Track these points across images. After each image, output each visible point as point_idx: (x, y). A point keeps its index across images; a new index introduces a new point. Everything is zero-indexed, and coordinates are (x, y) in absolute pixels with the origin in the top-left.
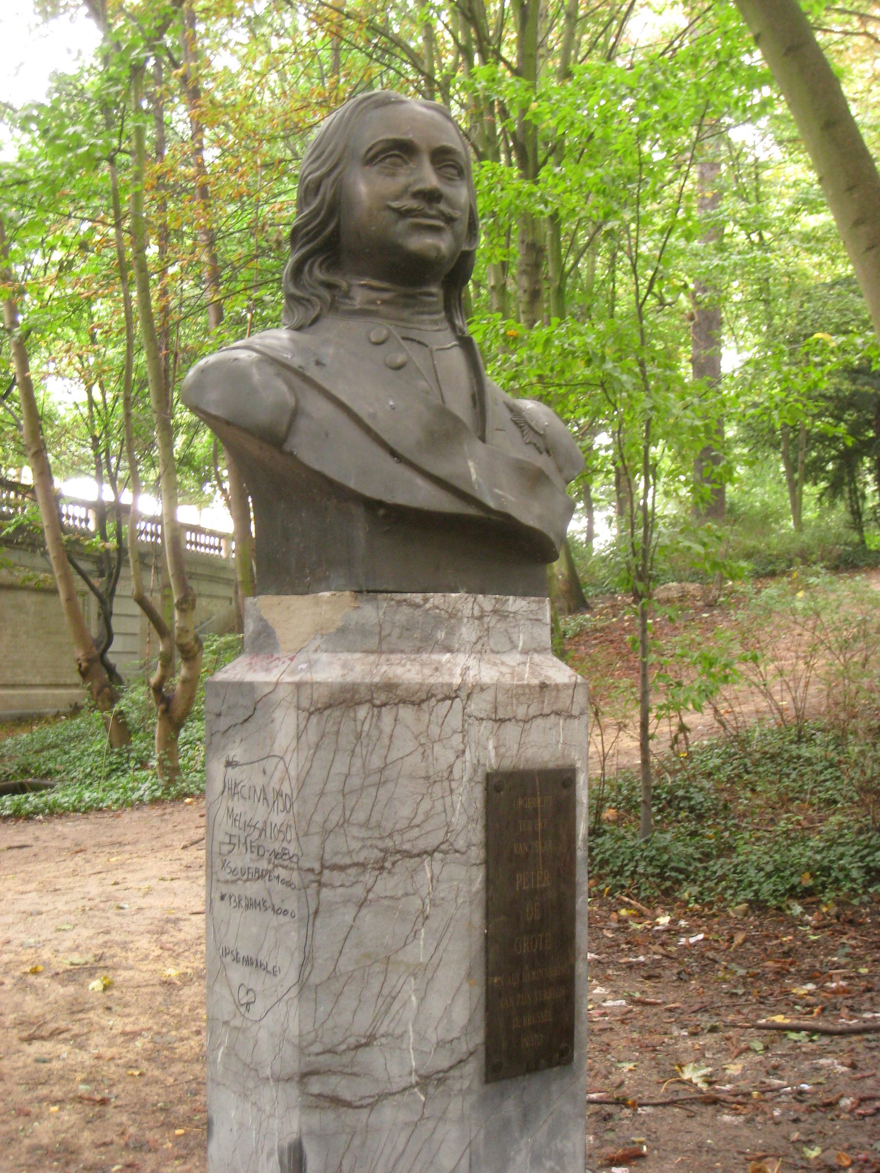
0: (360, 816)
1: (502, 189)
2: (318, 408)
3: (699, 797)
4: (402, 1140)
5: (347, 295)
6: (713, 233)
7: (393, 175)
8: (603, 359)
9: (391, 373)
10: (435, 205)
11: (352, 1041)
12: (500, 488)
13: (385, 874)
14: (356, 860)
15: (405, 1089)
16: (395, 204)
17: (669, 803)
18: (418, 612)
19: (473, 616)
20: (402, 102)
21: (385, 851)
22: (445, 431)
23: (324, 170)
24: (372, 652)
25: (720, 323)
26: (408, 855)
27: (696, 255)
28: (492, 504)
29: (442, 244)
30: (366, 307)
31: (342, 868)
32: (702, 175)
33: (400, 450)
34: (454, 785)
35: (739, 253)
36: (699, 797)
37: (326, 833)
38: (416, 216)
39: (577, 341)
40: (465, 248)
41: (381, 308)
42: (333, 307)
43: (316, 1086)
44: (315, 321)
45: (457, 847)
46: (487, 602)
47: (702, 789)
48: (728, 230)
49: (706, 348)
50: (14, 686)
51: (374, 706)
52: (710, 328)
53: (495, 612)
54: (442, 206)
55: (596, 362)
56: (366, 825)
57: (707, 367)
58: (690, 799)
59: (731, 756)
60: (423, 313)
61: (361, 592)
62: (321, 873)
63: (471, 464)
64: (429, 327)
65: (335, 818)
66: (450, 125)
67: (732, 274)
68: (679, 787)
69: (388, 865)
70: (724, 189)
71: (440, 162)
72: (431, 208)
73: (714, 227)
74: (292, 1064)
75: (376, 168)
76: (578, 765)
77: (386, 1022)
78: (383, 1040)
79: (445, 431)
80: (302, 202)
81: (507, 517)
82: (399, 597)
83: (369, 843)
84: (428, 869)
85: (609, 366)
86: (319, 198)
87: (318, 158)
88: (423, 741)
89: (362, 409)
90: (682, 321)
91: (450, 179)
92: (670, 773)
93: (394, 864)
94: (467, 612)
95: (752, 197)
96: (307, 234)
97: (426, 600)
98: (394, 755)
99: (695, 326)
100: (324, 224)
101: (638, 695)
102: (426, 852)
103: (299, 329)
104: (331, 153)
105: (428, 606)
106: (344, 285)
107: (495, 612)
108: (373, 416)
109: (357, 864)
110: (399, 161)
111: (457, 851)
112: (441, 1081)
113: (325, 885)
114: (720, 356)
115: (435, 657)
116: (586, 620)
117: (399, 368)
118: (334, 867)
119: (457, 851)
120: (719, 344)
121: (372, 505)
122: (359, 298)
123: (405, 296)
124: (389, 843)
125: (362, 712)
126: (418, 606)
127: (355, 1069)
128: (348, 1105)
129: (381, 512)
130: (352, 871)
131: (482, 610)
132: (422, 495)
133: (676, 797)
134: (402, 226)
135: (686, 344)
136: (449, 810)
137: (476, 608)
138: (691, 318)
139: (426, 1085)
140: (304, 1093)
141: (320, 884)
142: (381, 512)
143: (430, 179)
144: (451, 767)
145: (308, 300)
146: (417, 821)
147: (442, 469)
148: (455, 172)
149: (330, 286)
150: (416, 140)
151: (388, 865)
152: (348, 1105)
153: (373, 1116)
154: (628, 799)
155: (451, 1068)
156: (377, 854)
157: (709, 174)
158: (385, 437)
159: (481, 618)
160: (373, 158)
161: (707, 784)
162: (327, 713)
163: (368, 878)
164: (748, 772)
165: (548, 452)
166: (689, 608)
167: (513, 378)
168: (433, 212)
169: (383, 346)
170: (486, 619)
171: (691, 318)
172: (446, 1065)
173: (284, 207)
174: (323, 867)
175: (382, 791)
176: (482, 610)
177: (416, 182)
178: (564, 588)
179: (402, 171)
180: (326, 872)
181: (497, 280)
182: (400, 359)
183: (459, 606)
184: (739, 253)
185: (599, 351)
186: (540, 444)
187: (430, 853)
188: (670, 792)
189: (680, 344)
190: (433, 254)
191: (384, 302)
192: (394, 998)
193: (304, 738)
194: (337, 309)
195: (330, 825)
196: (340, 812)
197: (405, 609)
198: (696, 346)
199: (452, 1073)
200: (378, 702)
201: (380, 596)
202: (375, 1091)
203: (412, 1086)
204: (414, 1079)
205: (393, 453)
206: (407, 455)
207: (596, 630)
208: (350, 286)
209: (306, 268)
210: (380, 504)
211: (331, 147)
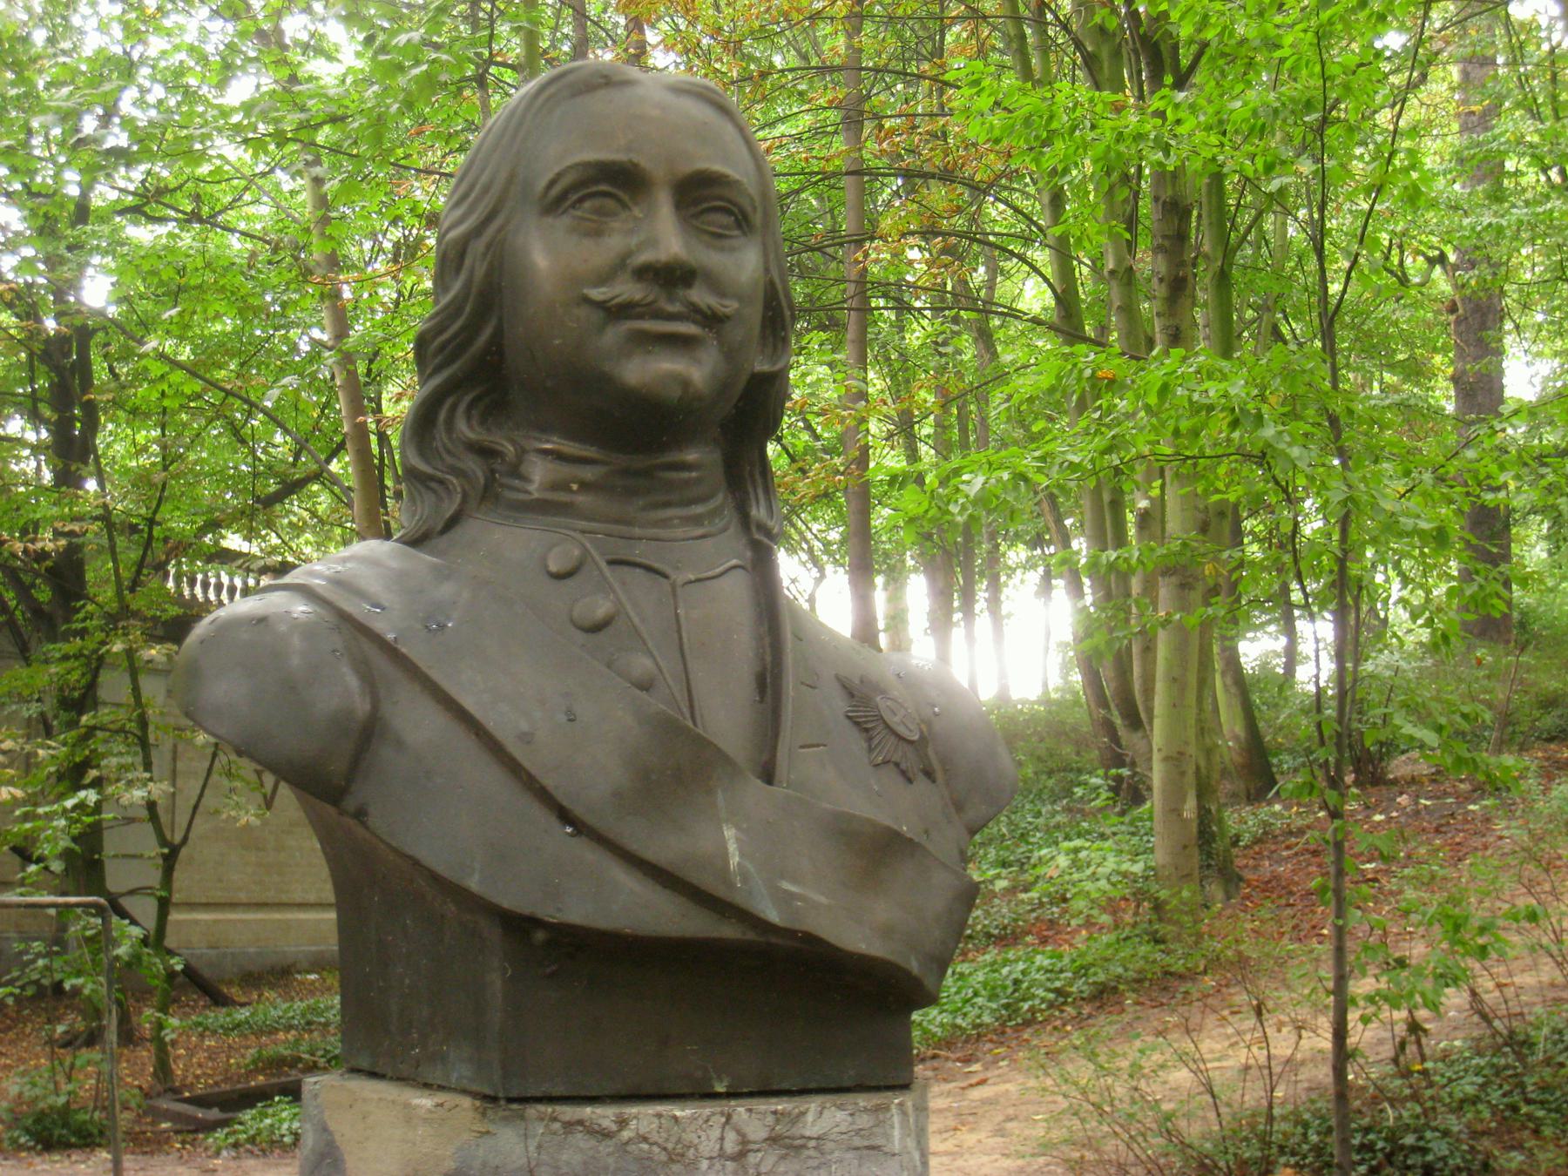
1: (1093, 127)
2: (416, 723)
3: (1440, 1148)
5: (515, 471)
6: (1486, 168)
7: (597, 233)
8: (1259, 420)
9: (581, 637)
10: (681, 292)
12: (794, 881)
16: (597, 294)
17: (1389, 1157)
18: (606, 1147)
19: (722, 1155)
20: (627, 83)
22: (679, 765)
25: (1502, 315)
27: (1456, 208)
28: (773, 916)
29: (696, 371)
30: (549, 496)
32: (1466, 75)
33: (578, 811)
35: (1527, 203)
36: (1440, 1148)
38: (640, 317)
39: (1213, 389)
40: (762, 366)
41: (581, 499)
42: (489, 494)
44: (452, 523)
46: (754, 1118)
47: (1446, 1133)
48: (1510, 165)
49: (1476, 359)
52: (1483, 326)
53: (773, 1140)
54: (700, 296)
55: (1247, 424)
57: (1481, 393)
58: (1424, 1151)
59: (1498, 1071)
60: (667, 505)
61: (493, 1099)
63: (729, 833)
64: (679, 532)
66: (729, 128)
67: (1516, 237)
68: (1407, 1128)
70: (1501, 99)
71: (696, 202)
72: (671, 300)
73: (1485, 159)
75: (565, 221)
79: (679, 765)
80: (441, 280)
81: (811, 939)
82: (569, 1112)
85: (1269, 432)
89: (503, 721)
90: (1437, 312)
91: (720, 236)
92: (1392, 1102)
94: (709, 1146)
95: (1547, 111)
96: (443, 347)
97: (622, 1123)
99: (1458, 322)
100: (472, 329)
101: (1330, 985)
103: (417, 541)
104: (486, 190)
105: (626, 1134)
106: (509, 449)
107: (773, 1140)
108: (526, 738)
110: (610, 204)
114: (1501, 373)
116: (1274, 814)
117: (597, 628)
120: (1499, 353)
121: (518, 926)
122: (539, 473)
123: (626, 472)
126: (606, 1135)
129: (540, 936)
131: (744, 1140)
132: (627, 904)
133: (1402, 1147)
134: (614, 334)
135: (1444, 350)
137: (731, 1136)
138: (1453, 309)
142: (540, 936)
143: (668, 237)
145: (441, 482)
147: (664, 848)
148: (730, 220)
149: (486, 453)
150: (644, 162)
154: (1318, 1150)
157: (1476, 73)
158: (548, 782)
159: (740, 1156)
160: (556, 202)
161: (1454, 1124)
164: (1528, 1102)
165: (929, 774)
166: (1446, 794)
167: (1109, 450)
168: (675, 308)
169: (570, 582)
170: (752, 1159)
171: (1453, 309)
173: (394, 295)
176: (744, 1140)
177: (641, 247)
178: (1238, 759)
179: (616, 225)
181: (1119, 260)
182: (602, 609)
183: (690, 1137)
184: (1527, 203)
185: (1251, 406)
186: (911, 762)
188: (1392, 1138)
189: (1435, 350)
190: (675, 393)
191: (585, 486)
194: (497, 497)
197: (579, 1139)
198: (1461, 355)
201: (532, 1111)
205: (565, 816)
206: (590, 819)
207: (1291, 833)
208: (522, 453)
209: (442, 415)
210: (534, 922)
211: (484, 179)
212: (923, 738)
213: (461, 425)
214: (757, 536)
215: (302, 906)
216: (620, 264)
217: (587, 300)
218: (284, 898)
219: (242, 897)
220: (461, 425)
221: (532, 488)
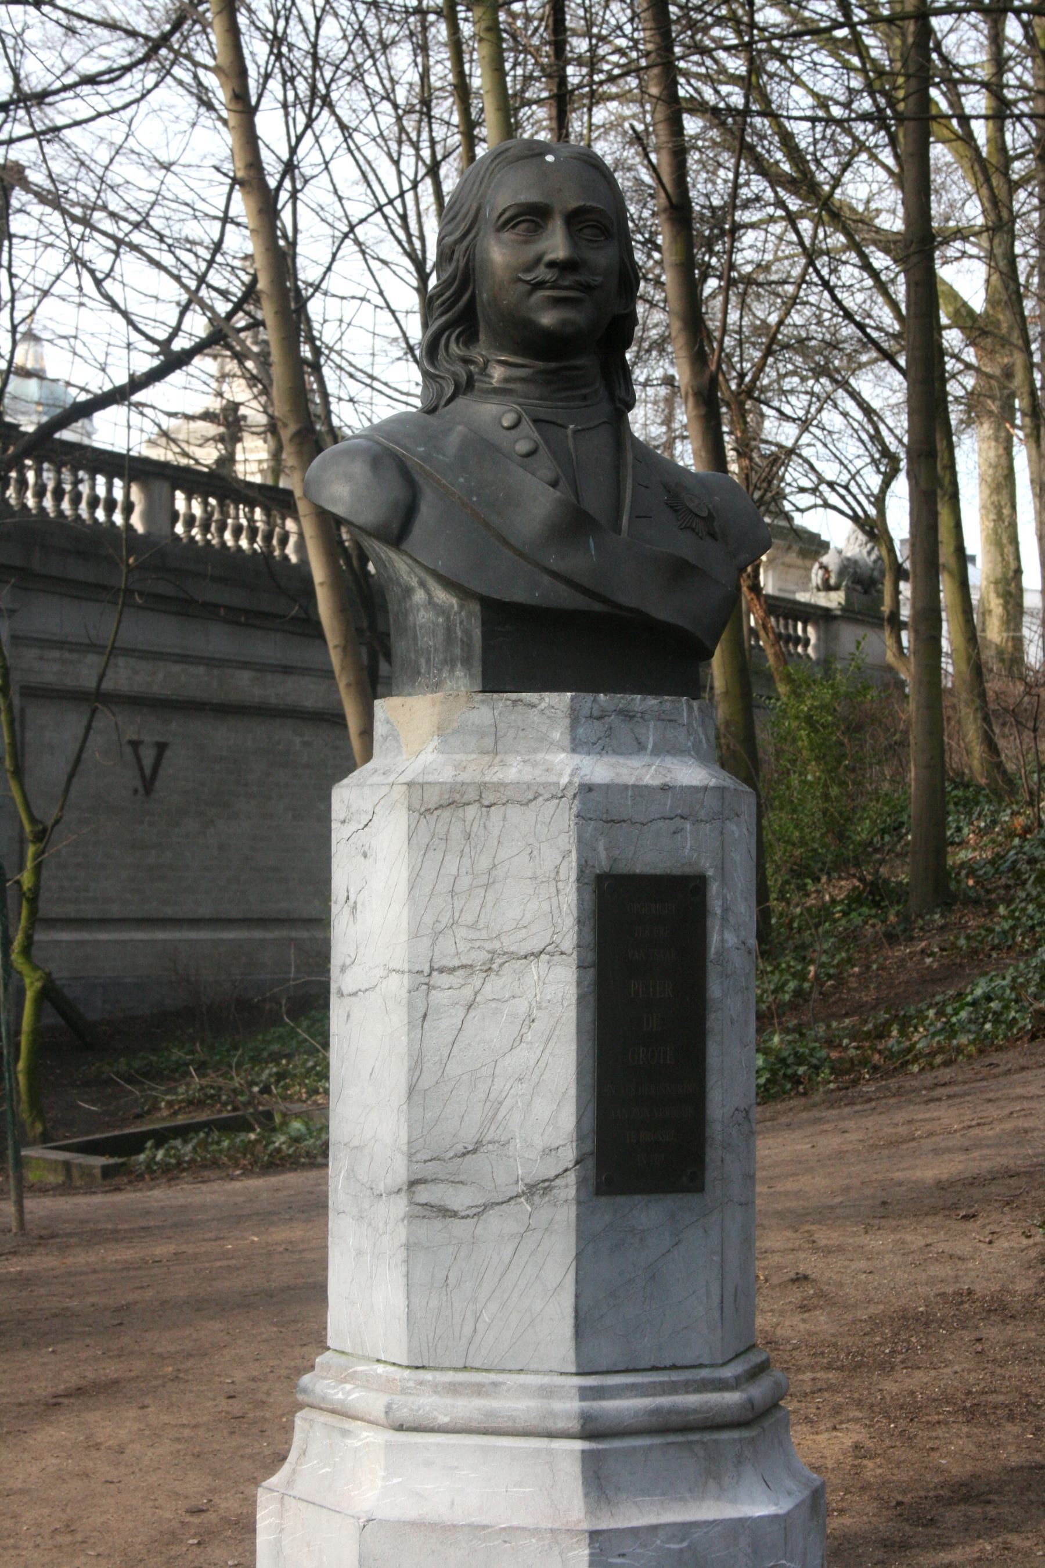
0: (468, 918)
4: (508, 1251)
11: (459, 1148)
13: (493, 975)
14: (465, 962)
15: (511, 1199)
21: (493, 952)
23: (457, 234)
24: (488, 753)
26: (514, 956)
31: (452, 970)
34: (561, 885)
37: (436, 935)
43: (424, 1194)
45: (563, 949)
50: (263, 922)
51: (483, 806)
56: (473, 927)
62: (430, 975)
65: (445, 920)
69: (495, 966)
74: (399, 1172)
76: (710, 873)
77: (493, 1128)
78: (490, 1146)
83: (477, 944)
84: (534, 970)
86: (454, 264)
87: (453, 219)
88: (531, 841)
93: (501, 965)
96: (443, 304)
98: (502, 855)
102: (532, 954)
109: (463, 967)
111: (562, 953)
112: (547, 1190)
113: (434, 988)
115: (549, 757)
118: (441, 970)
119: (562, 953)
122: (497, 373)
124: (496, 945)
125: (471, 811)
127: (462, 1178)
128: (454, 1214)
130: (460, 973)
136: (555, 912)
139: (533, 1195)
140: (411, 1203)
141: (430, 987)
144: (557, 868)
146: (524, 922)
151: (495, 966)
152: (454, 1214)
153: (480, 1227)
155: (557, 1176)
156: (485, 956)
162: (436, 813)
163: (477, 980)
172: (552, 1174)
174: (432, 969)
175: (491, 891)
180: (435, 973)
187: (537, 955)
192: (501, 1103)
193: (414, 838)
195: (440, 927)
196: (449, 913)
199: (558, 1182)
200: (487, 803)
202: (481, 1201)
203: (518, 1196)
204: (521, 1187)
209: (443, 342)
212: (710, 514)
213: (453, 346)
214: (619, 405)
215: (195, 922)
216: (538, 260)
217: (520, 280)
218: (169, 911)
219: (115, 910)
220: (453, 346)
221: (494, 381)
